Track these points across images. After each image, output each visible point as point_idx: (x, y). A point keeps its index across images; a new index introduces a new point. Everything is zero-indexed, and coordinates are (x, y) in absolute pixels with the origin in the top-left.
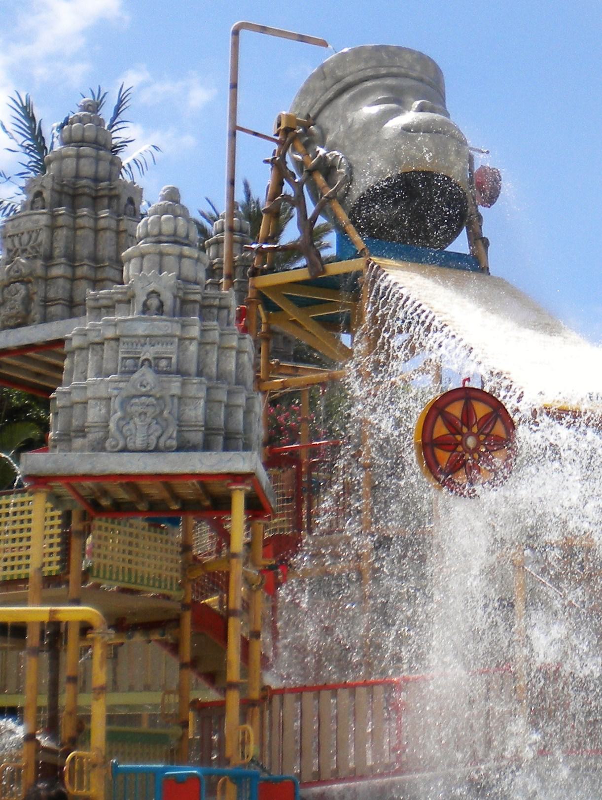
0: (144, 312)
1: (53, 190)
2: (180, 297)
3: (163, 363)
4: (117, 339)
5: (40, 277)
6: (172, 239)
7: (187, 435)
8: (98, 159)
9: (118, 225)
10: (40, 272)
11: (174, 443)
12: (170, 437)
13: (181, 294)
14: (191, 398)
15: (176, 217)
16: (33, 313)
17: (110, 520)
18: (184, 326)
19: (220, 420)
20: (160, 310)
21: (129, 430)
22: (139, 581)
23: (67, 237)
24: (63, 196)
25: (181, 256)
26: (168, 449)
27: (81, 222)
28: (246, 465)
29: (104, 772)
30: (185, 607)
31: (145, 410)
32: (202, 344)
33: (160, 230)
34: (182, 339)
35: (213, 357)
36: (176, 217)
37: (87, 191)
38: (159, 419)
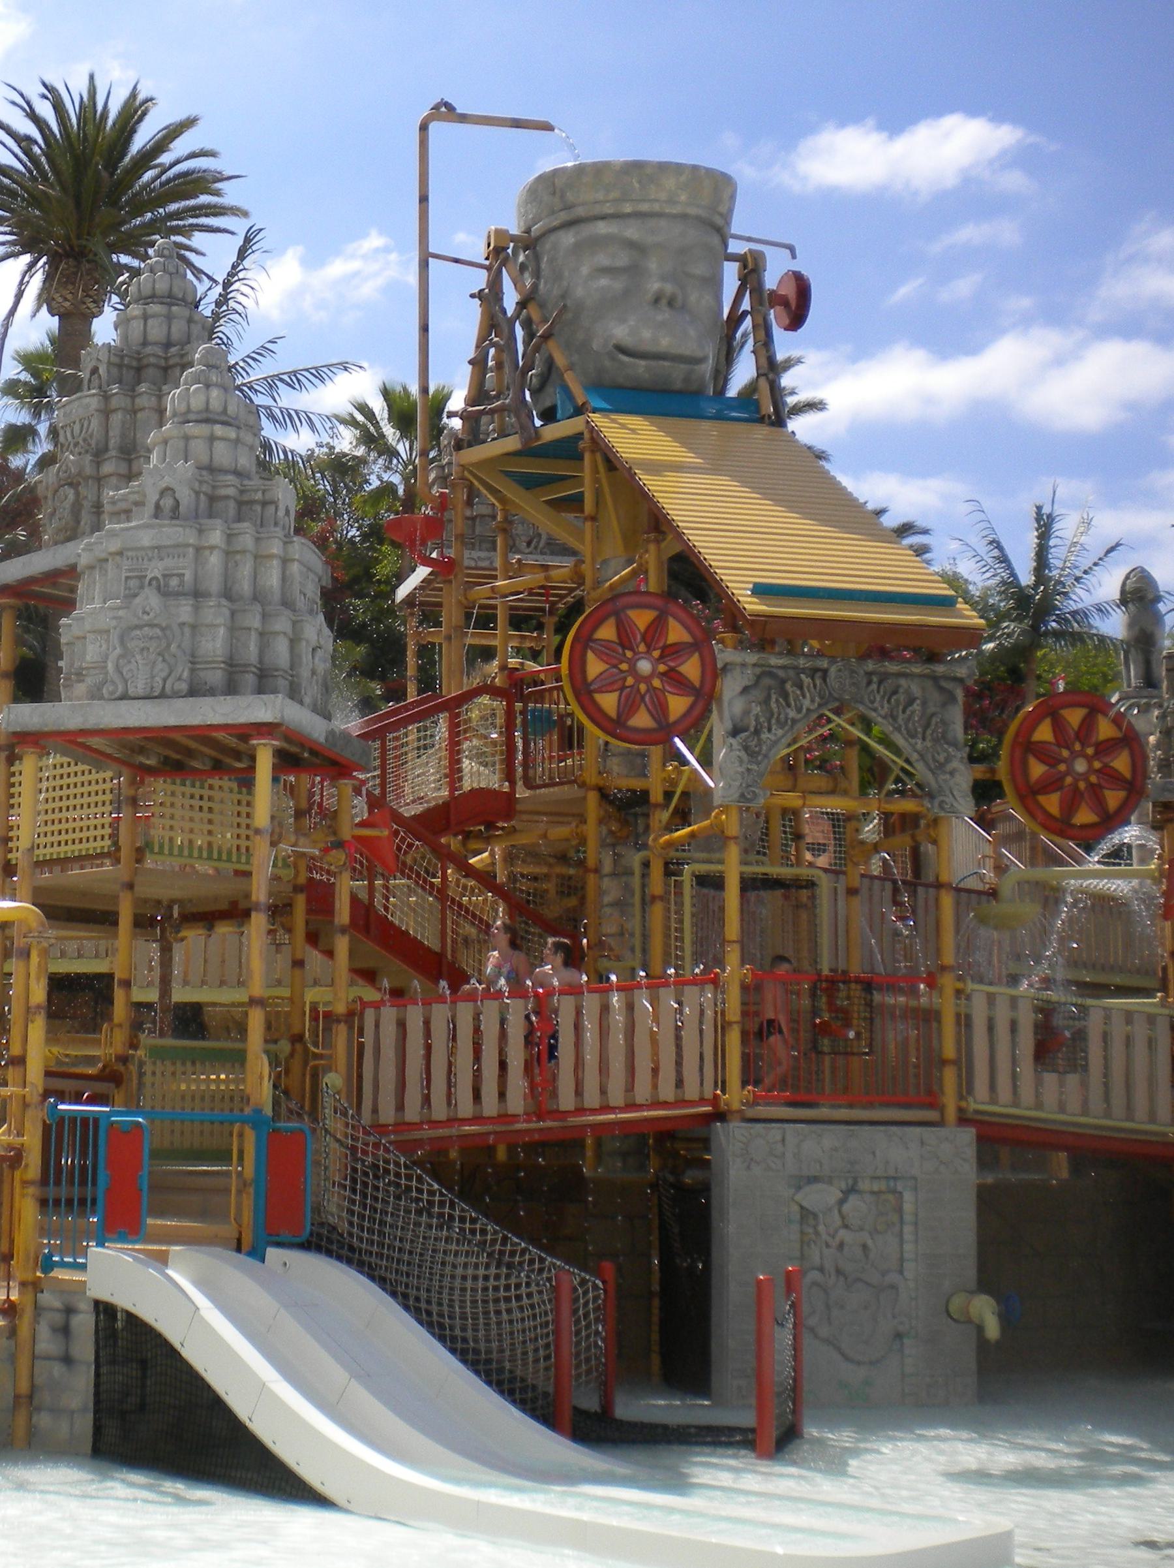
0: (156, 516)
1: (109, 363)
2: (205, 494)
3: (174, 582)
4: (120, 553)
5: (89, 477)
6: (204, 416)
7: (202, 674)
8: (169, 318)
9: (133, 403)
10: (89, 470)
11: (184, 687)
12: (180, 679)
13: (205, 488)
14: (207, 626)
15: (208, 386)
16: (82, 523)
17: (178, 781)
18: (201, 531)
19: (251, 651)
20: (175, 513)
21: (131, 670)
22: (224, 857)
23: (123, 423)
24: (124, 371)
25: (212, 439)
26: (177, 695)
27: (139, 402)
28: (269, 712)
29: (40, 1115)
30: (297, 889)
31: (147, 645)
32: (228, 554)
33: (189, 406)
34: (198, 550)
35: (246, 570)
36: (208, 386)
37: (152, 360)
38: (167, 657)
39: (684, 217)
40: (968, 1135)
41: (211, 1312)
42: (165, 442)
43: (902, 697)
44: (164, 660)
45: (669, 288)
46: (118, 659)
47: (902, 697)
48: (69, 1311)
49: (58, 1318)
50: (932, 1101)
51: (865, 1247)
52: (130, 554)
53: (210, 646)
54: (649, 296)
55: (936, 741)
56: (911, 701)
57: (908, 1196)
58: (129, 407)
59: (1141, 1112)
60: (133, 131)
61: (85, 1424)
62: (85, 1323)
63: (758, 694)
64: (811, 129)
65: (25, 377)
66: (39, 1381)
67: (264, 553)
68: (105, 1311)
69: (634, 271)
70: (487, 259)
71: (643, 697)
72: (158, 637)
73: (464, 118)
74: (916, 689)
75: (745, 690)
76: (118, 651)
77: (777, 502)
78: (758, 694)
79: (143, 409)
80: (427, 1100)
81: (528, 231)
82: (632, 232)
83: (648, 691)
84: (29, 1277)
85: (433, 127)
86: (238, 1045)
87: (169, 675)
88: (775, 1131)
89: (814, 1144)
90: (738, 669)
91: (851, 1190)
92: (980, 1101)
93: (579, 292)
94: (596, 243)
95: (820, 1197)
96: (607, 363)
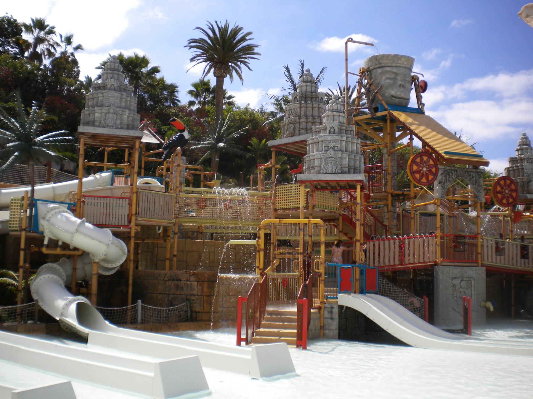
3: (336, 148)
4: (322, 141)
8: (312, 86)
10: (298, 120)
25: (339, 116)
26: (338, 173)
36: (337, 104)
39: (405, 67)
40: (484, 269)
41: (374, 308)
42: (328, 116)
43: (471, 176)
45: (403, 83)
47: (471, 176)
48: (332, 308)
49: (330, 310)
50: (476, 262)
51: (465, 292)
54: (398, 85)
55: (478, 186)
56: (473, 177)
57: (473, 281)
59: (511, 263)
60: (237, 34)
61: (336, 332)
62: (336, 310)
63: (444, 175)
64: (333, 36)
65: (195, 90)
66: (325, 323)
68: (341, 307)
69: (395, 79)
73: (355, 42)
74: (474, 175)
75: (442, 174)
77: (437, 133)
78: (444, 175)
80: (389, 261)
81: (369, 68)
82: (395, 70)
84: (322, 301)
85: (349, 43)
86: (318, 249)
88: (448, 268)
89: (456, 271)
91: (462, 280)
92: (485, 263)
93: (383, 83)
94: (386, 72)
95: (456, 282)
96: (389, 99)
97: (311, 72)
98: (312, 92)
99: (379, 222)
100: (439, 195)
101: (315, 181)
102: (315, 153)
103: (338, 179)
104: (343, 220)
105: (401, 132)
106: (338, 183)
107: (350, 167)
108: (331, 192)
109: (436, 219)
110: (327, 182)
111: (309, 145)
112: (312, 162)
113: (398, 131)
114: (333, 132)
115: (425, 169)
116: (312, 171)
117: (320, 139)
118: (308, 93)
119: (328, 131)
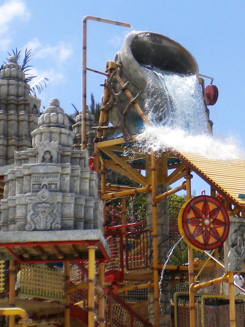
0: (43, 162)
3: (53, 186)
4: (30, 175)
6: (56, 124)
7: (65, 222)
8: (18, 86)
11: (59, 226)
13: (61, 152)
15: (57, 114)
18: (63, 168)
19: (82, 214)
20: (51, 160)
22: (47, 295)
25: (61, 133)
26: (56, 229)
27: (11, 117)
28: (95, 236)
32: (72, 177)
33: (50, 120)
36: (57, 114)
37: (13, 102)
38: (52, 215)
42: (41, 134)
44: (51, 216)
46: (31, 216)
52: (34, 175)
53: (68, 211)
58: (6, 119)
63: (239, 232)
67: (85, 177)
70: (107, 72)
71: (210, 232)
72: (48, 207)
75: (235, 231)
76: (32, 212)
78: (239, 232)
79: (12, 120)
83: (210, 230)
87: (53, 222)
90: (233, 223)
97: (61, 106)
98: (18, 96)
99: (140, 319)
100: (231, 265)
101: (16, 244)
102: (17, 195)
103: (55, 239)
104: (71, 315)
105: (175, 169)
106: (57, 248)
107: (77, 220)
108: (51, 266)
109: (228, 308)
110: (38, 245)
111: (8, 182)
112: (11, 211)
113: (170, 168)
114: (48, 159)
115: (207, 222)
116: (12, 227)
117: (26, 172)
118: (12, 97)
119: (40, 158)
